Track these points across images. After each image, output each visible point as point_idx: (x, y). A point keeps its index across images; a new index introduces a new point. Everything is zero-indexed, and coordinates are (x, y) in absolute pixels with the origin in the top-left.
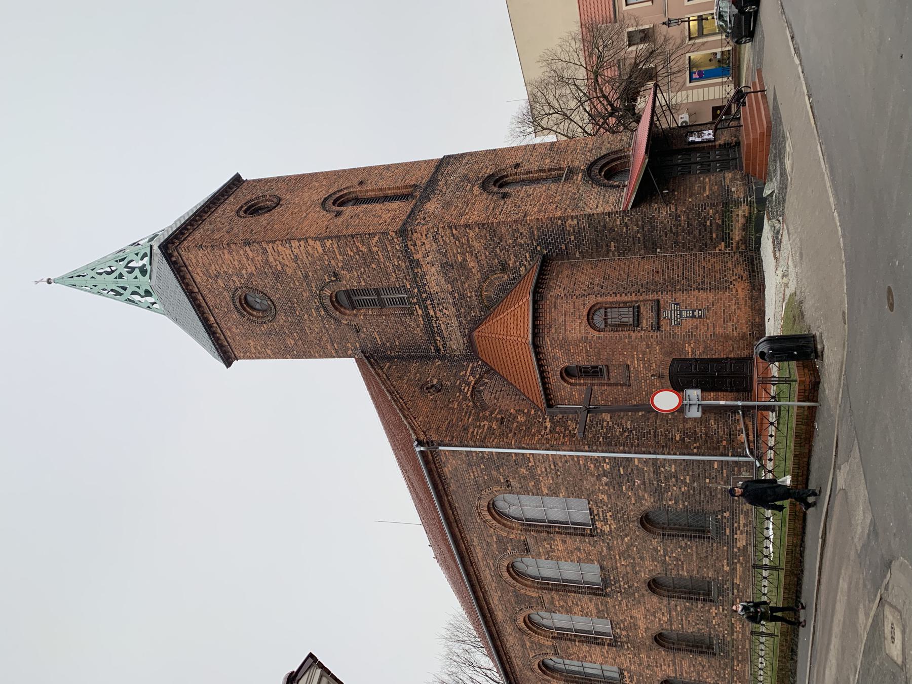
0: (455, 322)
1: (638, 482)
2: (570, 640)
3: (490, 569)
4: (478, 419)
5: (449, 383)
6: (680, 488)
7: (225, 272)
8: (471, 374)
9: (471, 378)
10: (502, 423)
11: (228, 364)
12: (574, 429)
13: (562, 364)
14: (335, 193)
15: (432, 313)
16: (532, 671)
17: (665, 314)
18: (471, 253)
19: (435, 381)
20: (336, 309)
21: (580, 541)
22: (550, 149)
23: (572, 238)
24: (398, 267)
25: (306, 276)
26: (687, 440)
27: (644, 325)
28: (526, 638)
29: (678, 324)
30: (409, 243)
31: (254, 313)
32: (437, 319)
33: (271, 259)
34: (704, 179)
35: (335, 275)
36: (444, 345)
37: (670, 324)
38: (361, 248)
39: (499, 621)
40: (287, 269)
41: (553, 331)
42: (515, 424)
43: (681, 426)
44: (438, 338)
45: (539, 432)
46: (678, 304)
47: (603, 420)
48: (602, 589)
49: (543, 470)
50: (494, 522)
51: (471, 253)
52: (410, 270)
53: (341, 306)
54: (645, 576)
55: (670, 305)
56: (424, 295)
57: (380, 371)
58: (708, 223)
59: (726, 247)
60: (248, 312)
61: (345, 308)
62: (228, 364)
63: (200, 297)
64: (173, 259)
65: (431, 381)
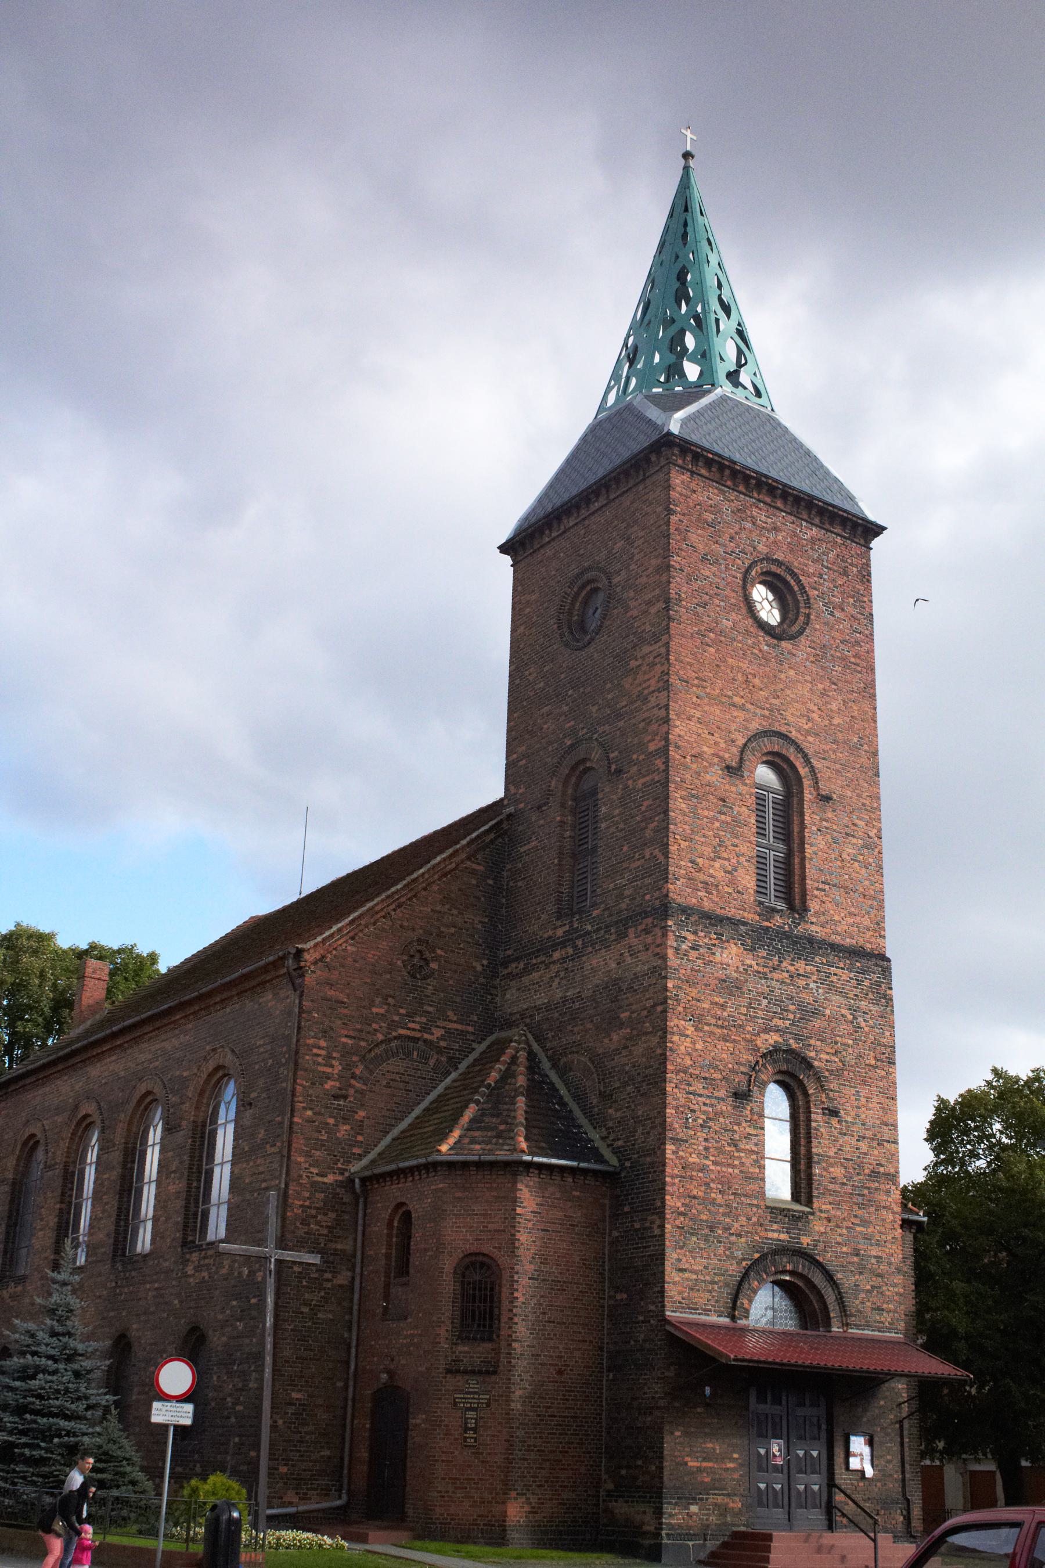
0: (541, 999)
1: (240, 1325)
2: (63, 1194)
3: (150, 1061)
4: (346, 1052)
5: (429, 992)
6: (230, 1395)
7: (633, 555)
8: (448, 1032)
9: (438, 1033)
10: (336, 1097)
11: (504, 549)
12: (318, 1223)
13: (418, 1208)
14: (799, 749)
15: (557, 955)
16: (27, 1123)
17: (473, 1384)
18: (630, 1039)
19: (434, 965)
20: (573, 768)
21: (178, 1223)
22: (875, 1174)
23: (637, 1226)
24: (621, 896)
25: (619, 715)
26: (291, 1410)
27: (461, 1348)
28: (66, 1114)
29: (455, 1404)
30: (649, 920)
31: (577, 605)
32: (547, 967)
33: (646, 649)
34: (734, 1460)
35: (619, 772)
36: (510, 976)
37: (456, 1391)
38: (652, 826)
39: (89, 1069)
40: (630, 679)
41: (459, 1194)
42: (332, 1121)
43: (320, 1401)
44: (521, 965)
45: (316, 1163)
46: (488, 1405)
47: (335, 1273)
48: (124, 1255)
49: (261, 1169)
50: (204, 1076)
51: (630, 1039)
52: (615, 918)
53: (580, 778)
54: (135, 1330)
55: (486, 1392)
56: (579, 943)
57: (463, 856)
58: (640, 1463)
59: (609, 1491)
60: (578, 594)
61: (577, 785)
62: (504, 549)
63: (602, 501)
64: (653, 458)
65: (436, 959)
